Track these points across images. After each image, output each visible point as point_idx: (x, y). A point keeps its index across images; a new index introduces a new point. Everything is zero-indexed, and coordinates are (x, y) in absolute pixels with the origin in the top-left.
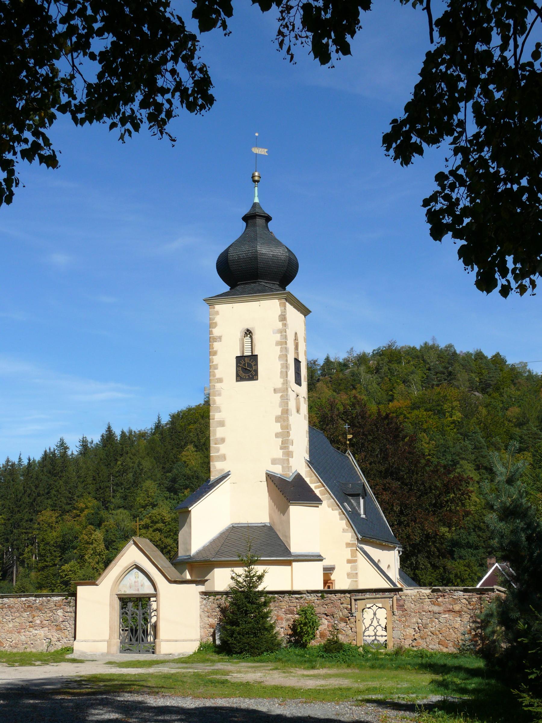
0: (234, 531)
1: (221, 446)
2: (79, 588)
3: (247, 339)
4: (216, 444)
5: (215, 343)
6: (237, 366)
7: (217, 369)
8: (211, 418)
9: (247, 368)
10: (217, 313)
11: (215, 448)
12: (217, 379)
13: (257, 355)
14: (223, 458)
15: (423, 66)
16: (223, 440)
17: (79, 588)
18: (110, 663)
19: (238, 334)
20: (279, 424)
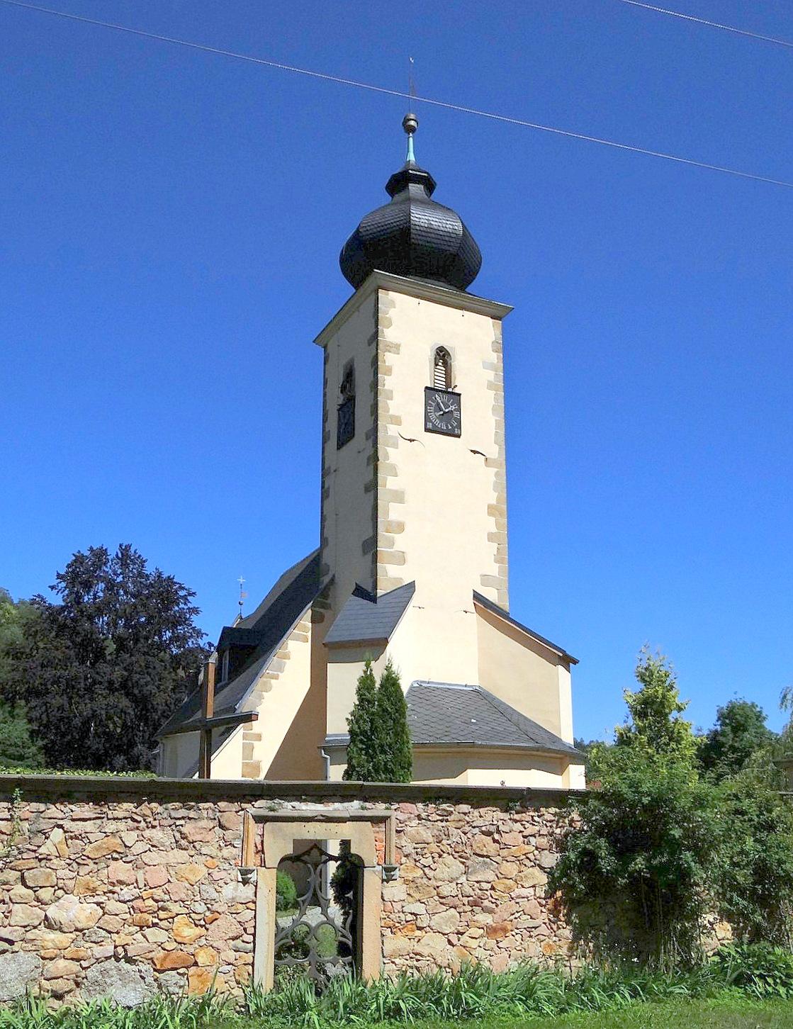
9: (443, 412)
13: (459, 395)
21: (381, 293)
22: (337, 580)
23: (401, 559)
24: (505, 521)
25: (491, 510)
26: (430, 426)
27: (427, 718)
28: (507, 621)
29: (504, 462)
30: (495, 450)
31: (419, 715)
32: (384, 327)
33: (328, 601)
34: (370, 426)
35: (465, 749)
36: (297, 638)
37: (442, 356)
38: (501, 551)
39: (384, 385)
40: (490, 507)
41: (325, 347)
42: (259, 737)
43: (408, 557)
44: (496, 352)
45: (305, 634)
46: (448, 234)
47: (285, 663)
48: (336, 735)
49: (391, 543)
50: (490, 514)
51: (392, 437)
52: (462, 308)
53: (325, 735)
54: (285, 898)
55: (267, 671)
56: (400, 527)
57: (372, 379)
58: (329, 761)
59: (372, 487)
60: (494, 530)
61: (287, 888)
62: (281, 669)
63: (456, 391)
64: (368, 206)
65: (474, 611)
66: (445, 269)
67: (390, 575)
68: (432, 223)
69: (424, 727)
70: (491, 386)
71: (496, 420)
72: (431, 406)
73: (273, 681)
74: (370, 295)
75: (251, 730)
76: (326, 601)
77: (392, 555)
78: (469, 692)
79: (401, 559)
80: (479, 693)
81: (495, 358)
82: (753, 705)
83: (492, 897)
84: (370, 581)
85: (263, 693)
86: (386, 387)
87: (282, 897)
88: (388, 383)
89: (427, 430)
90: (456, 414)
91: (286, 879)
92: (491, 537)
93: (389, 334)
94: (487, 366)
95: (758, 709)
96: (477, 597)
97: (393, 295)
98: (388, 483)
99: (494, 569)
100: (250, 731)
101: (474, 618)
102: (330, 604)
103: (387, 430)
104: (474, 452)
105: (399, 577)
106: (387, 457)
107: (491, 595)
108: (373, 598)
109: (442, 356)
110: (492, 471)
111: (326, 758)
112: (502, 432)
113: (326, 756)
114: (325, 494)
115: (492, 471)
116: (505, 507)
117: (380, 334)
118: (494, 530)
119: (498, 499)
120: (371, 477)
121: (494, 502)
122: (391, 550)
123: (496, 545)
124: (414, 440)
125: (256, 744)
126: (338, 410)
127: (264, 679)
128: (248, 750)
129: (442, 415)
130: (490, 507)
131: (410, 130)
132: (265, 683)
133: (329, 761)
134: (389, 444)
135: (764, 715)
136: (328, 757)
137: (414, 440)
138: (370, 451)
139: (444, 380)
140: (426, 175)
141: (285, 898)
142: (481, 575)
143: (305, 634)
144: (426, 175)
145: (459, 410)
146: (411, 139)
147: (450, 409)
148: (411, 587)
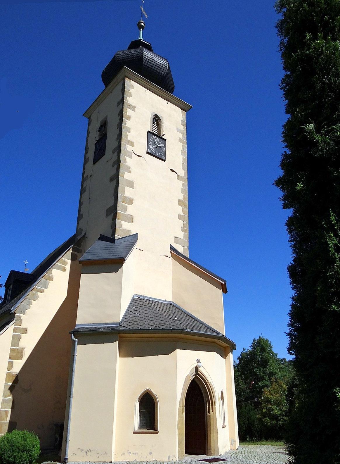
9: (156, 145)
11: (122, 206)
13: (165, 140)
21: (127, 80)
22: (87, 236)
23: (130, 219)
24: (187, 210)
25: (180, 202)
26: (149, 151)
27: (146, 315)
28: (191, 263)
29: (187, 180)
30: (182, 172)
31: (140, 313)
32: (127, 96)
33: (81, 248)
34: (116, 144)
35: (177, 335)
36: (59, 268)
37: (157, 120)
38: (185, 225)
39: (126, 124)
40: (179, 201)
41: (89, 118)
42: (25, 331)
43: (135, 219)
44: (183, 125)
45: (64, 266)
46: (162, 65)
47: (49, 283)
48: (82, 325)
49: (125, 210)
50: (180, 204)
51: (128, 151)
52: (167, 100)
53: (75, 325)
54: (30, 456)
55: (36, 287)
56: (131, 202)
57: (118, 121)
58: (76, 343)
59: (116, 178)
60: (182, 213)
61: (33, 447)
62: (46, 286)
63: (164, 137)
64: (121, 48)
65: (171, 257)
66: (161, 82)
67: (124, 227)
68: (154, 57)
69: (146, 320)
70: (180, 140)
71: (183, 158)
72: (150, 141)
73: (40, 294)
74: (119, 82)
75: (20, 326)
76: (80, 248)
77: (126, 216)
78: (167, 305)
79: (130, 219)
80: (172, 305)
81: (183, 128)
82: (267, 340)
83: (247, 453)
84: (111, 231)
85: (32, 301)
86: (126, 126)
87: (29, 455)
88: (128, 124)
89: (148, 153)
90: (163, 149)
91: (33, 439)
92: (180, 217)
93: (129, 100)
94: (178, 130)
95: (269, 342)
96: (172, 248)
97: (132, 82)
98: (125, 176)
99: (182, 235)
100: (20, 327)
101: (170, 261)
102: (81, 250)
103: (126, 148)
104: (172, 171)
105: (129, 229)
106: (125, 161)
107: (180, 249)
108: (112, 240)
109: (157, 120)
110: (181, 183)
111: (75, 341)
112: (186, 164)
113: (75, 339)
114: (83, 190)
115: (181, 183)
116: (187, 202)
117: (125, 98)
118: (182, 213)
119: (184, 197)
120: (115, 171)
121: (182, 199)
122: (125, 213)
123: (182, 222)
124: (141, 156)
125: (23, 335)
126: (96, 144)
127: (33, 292)
128: (16, 340)
129: (156, 147)
130: (179, 201)
131: (140, 27)
132: (34, 295)
133: (76, 343)
134: (127, 155)
135: (271, 345)
136: (76, 339)
137: (141, 156)
138: (115, 158)
139: (157, 132)
140: (149, 44)
141: (30, 456)
142: (174, 237)
143: (64, 266)
144: (149, 44)
145: (165, 147)
146: (141, 32)
147: (160, 145)
148: (135, 237)
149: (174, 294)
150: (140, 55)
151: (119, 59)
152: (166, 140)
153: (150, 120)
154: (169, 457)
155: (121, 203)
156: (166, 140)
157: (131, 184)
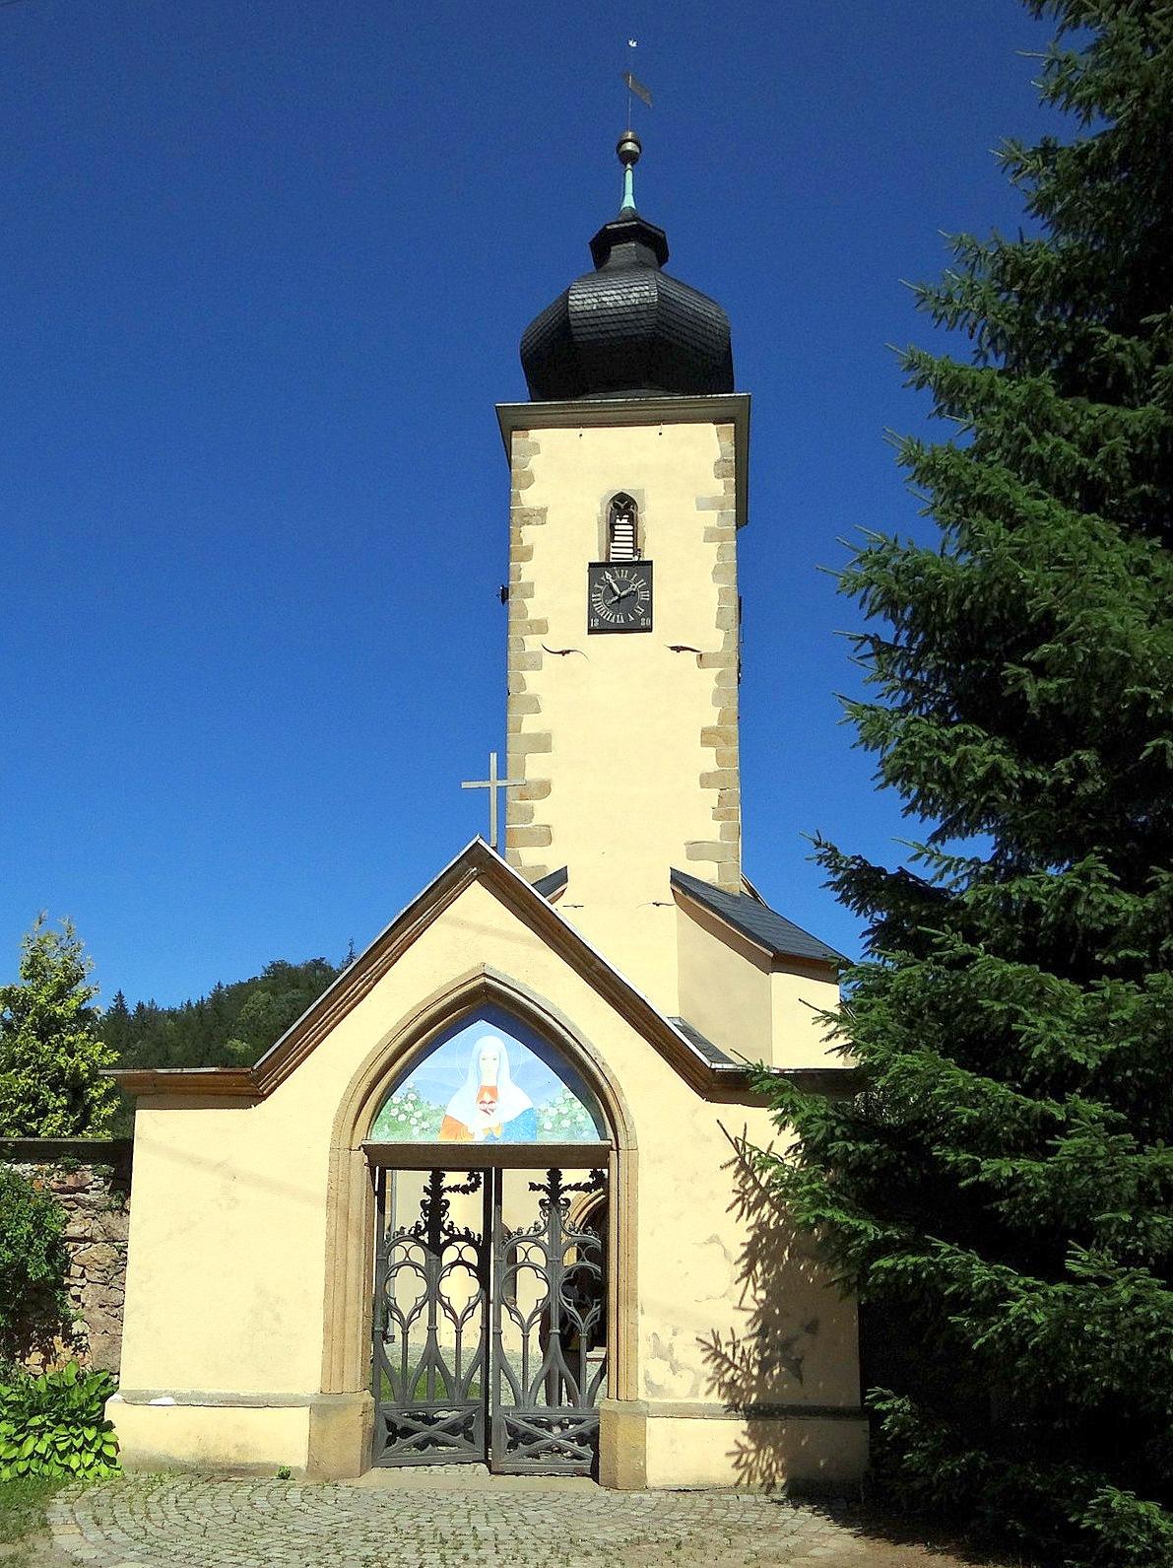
0: (245, 1088)
1: (538, 805)
2: (152, 1126)
3: (623, 526)
4: (522, 798)
5: (525, 528)
6: (591, 590)
7: (532, 596)
8: (510, 726)
9: (621, 597)
10: (535, 448)
11: (520, 808)
12: (531, 624)
13: (650, 563)
14: (545, 836)
15: (482, 1024)
16: (544, 789)
17: (152, 1126)
18: (861, 606)
19: (595, 509)
20: (712, 751)
88: (526, 571)
92: (706, 780)
101: (673, 915)
104: (678, 649)
105: (541, 864)
106: (522, 684)
107: (706, 872)
116: (734, 728)
124: (568, 652)
137: (568, 652)
140: (635, 223)
145: (649, 587)
146: (629, 175)
149: (684, 998)
150: (531, 352)
151: (548, 334)
152: (651, 562)
153: (599, 523)
154: (865, 1431)
155: (516, 804)
156: (651, 562)
157: (542, 743)
